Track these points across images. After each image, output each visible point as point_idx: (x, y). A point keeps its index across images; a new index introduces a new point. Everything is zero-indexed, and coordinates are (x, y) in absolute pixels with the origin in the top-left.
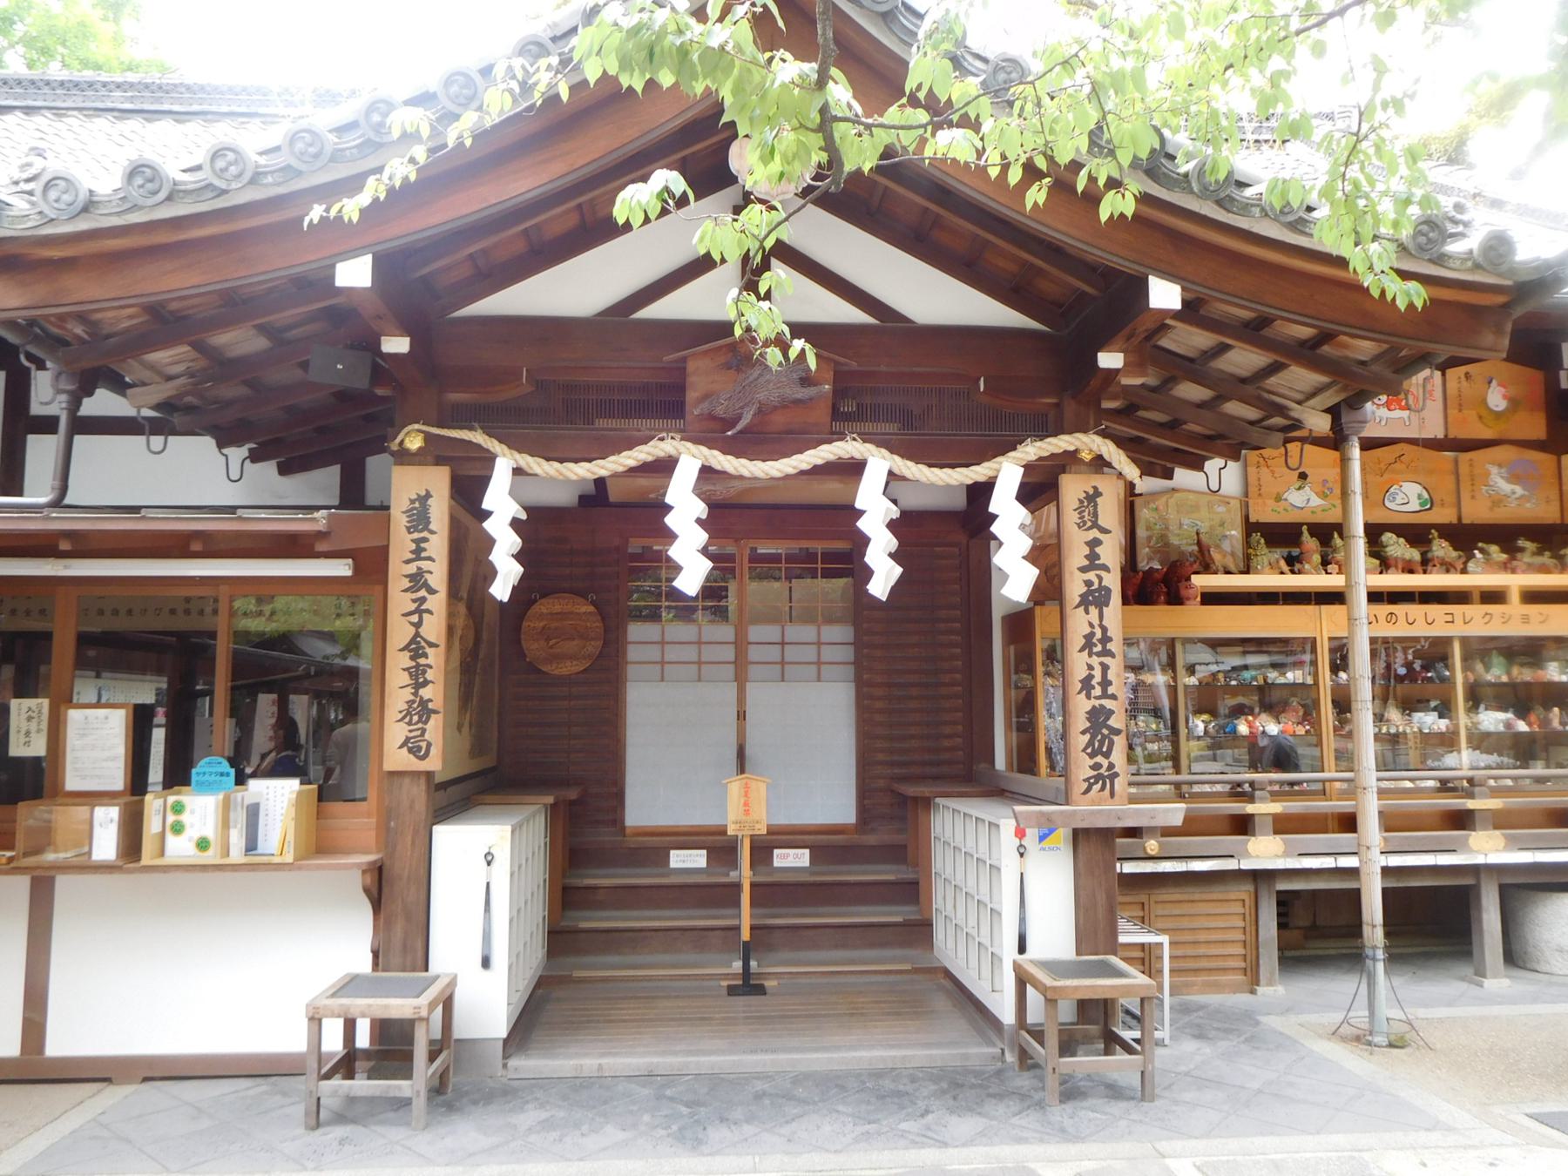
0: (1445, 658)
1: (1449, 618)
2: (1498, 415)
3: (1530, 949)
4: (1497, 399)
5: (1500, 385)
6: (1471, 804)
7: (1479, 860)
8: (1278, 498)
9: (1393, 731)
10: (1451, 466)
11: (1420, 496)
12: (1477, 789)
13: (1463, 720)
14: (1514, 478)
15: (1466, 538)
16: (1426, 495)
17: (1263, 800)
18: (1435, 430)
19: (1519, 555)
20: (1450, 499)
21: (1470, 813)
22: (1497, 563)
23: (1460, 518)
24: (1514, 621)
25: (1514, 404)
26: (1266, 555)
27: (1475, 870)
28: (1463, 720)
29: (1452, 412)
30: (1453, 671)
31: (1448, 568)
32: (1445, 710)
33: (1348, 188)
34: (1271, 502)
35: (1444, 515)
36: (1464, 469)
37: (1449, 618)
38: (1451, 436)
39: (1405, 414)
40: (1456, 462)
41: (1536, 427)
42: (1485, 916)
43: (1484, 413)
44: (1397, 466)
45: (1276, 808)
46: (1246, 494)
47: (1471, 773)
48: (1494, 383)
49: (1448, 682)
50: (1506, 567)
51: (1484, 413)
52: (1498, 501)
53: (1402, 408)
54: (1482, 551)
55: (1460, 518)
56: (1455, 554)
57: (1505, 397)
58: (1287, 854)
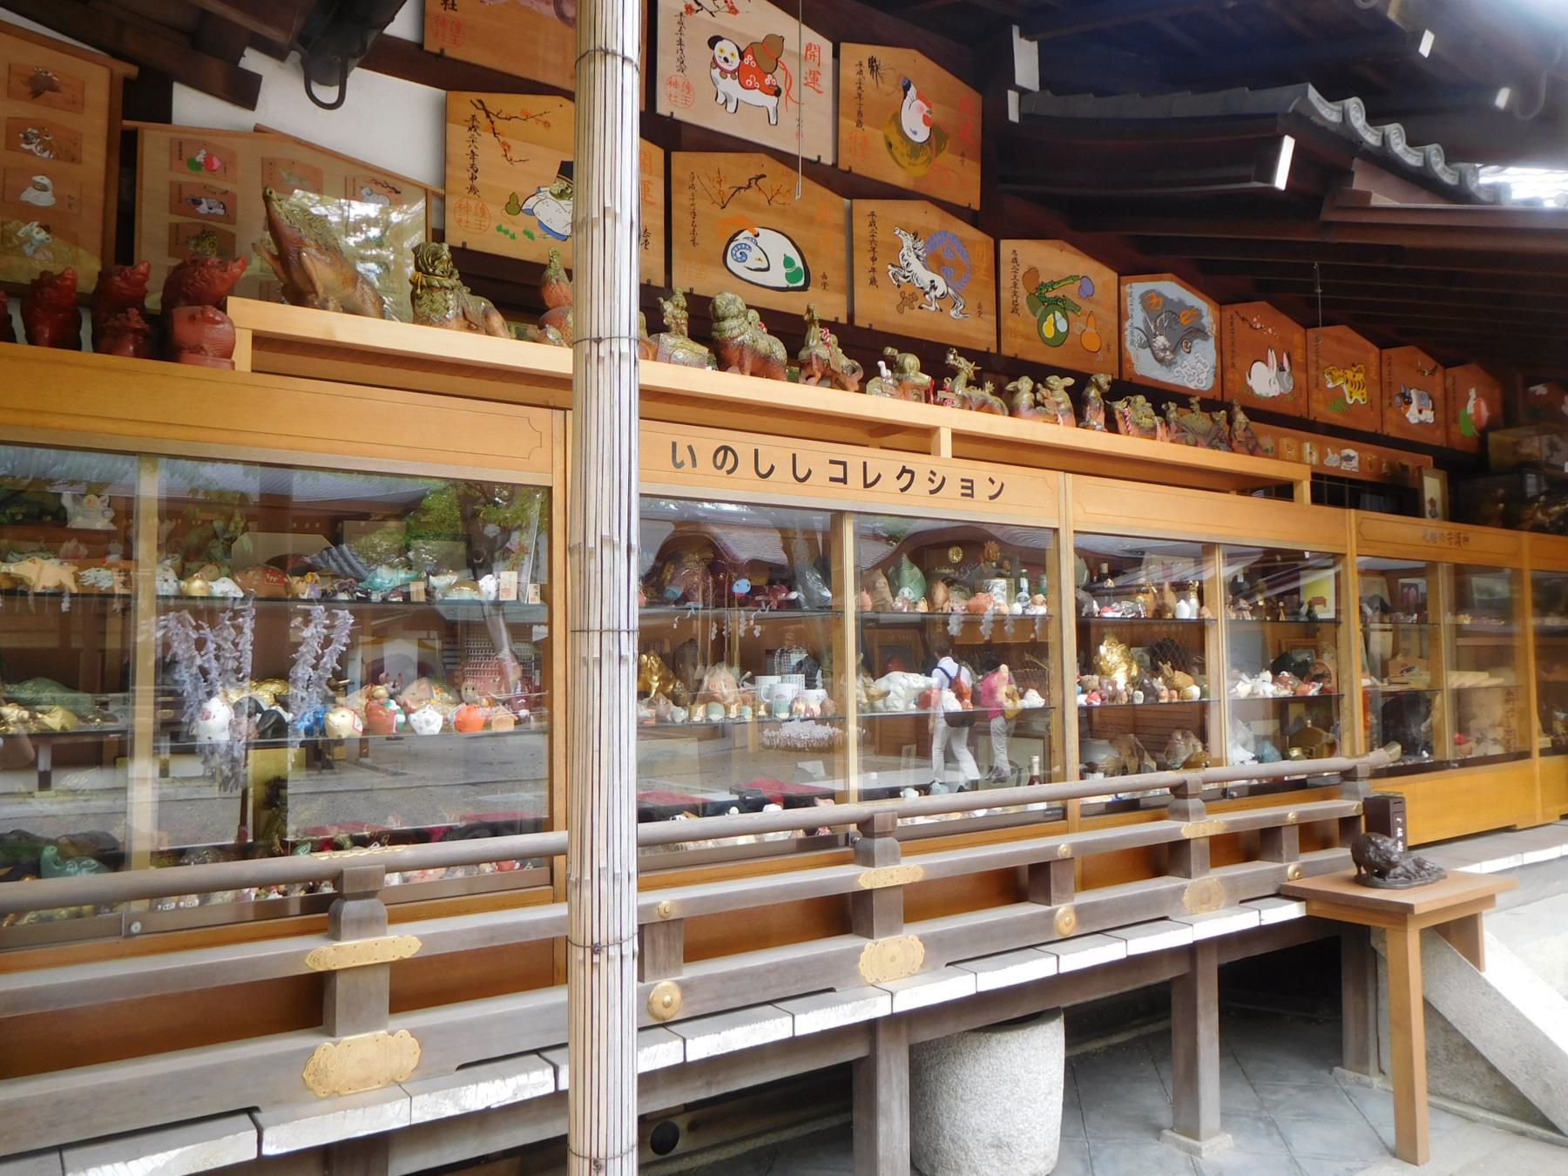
0: (825, 566)
1: (838, 471)
2: (916, 149)
3: (945, 1145)
4: (914, 121)
5: (920, 96)
6: (865, 878)
7: (879, 1008)
8: (514, 206)
9: (717, 716)
10: (839, 218)
11: (788, 262)
12: (878, 843)
13: (854, 686)
14: (935, 262)
15: (867, 350)
16: (799, 263)
17: (365, 925)
18: (818, 148)
19: (948, 382)
20: (837, 277)
21: (865, 897)
22: (917, 387)
23: (851, 317)
24: (941, 493)
25: (938, 134)
26: (455, 298)
27: (870, 1029)
28: (854, 686)
29: (847, 123)
30: (839, 592)
31: (832, 379)
32: (818, 665)
33: (762, 713)
34: (496, 211)
35: (826, 304)
36: (861, 229)
37: (838, 471)
38: (843, 166)
39: (770, 101)
40: (850, 214)
41: (965, 184)
42: (882, 1127)
43: (895, 139)
44: (751, 194)
45: (402, 942)
46: (443, 180)
47: (867, 808)
48: (912, 91)
49: (833, 613)
50: (929, 396)
51: (895, 139)
52: (911, 297)
53: (766, 90)
54: (892, 364)
55: (851, 317)
56: (845, 362)
57: (926, 120)
58: (427, 1075)
